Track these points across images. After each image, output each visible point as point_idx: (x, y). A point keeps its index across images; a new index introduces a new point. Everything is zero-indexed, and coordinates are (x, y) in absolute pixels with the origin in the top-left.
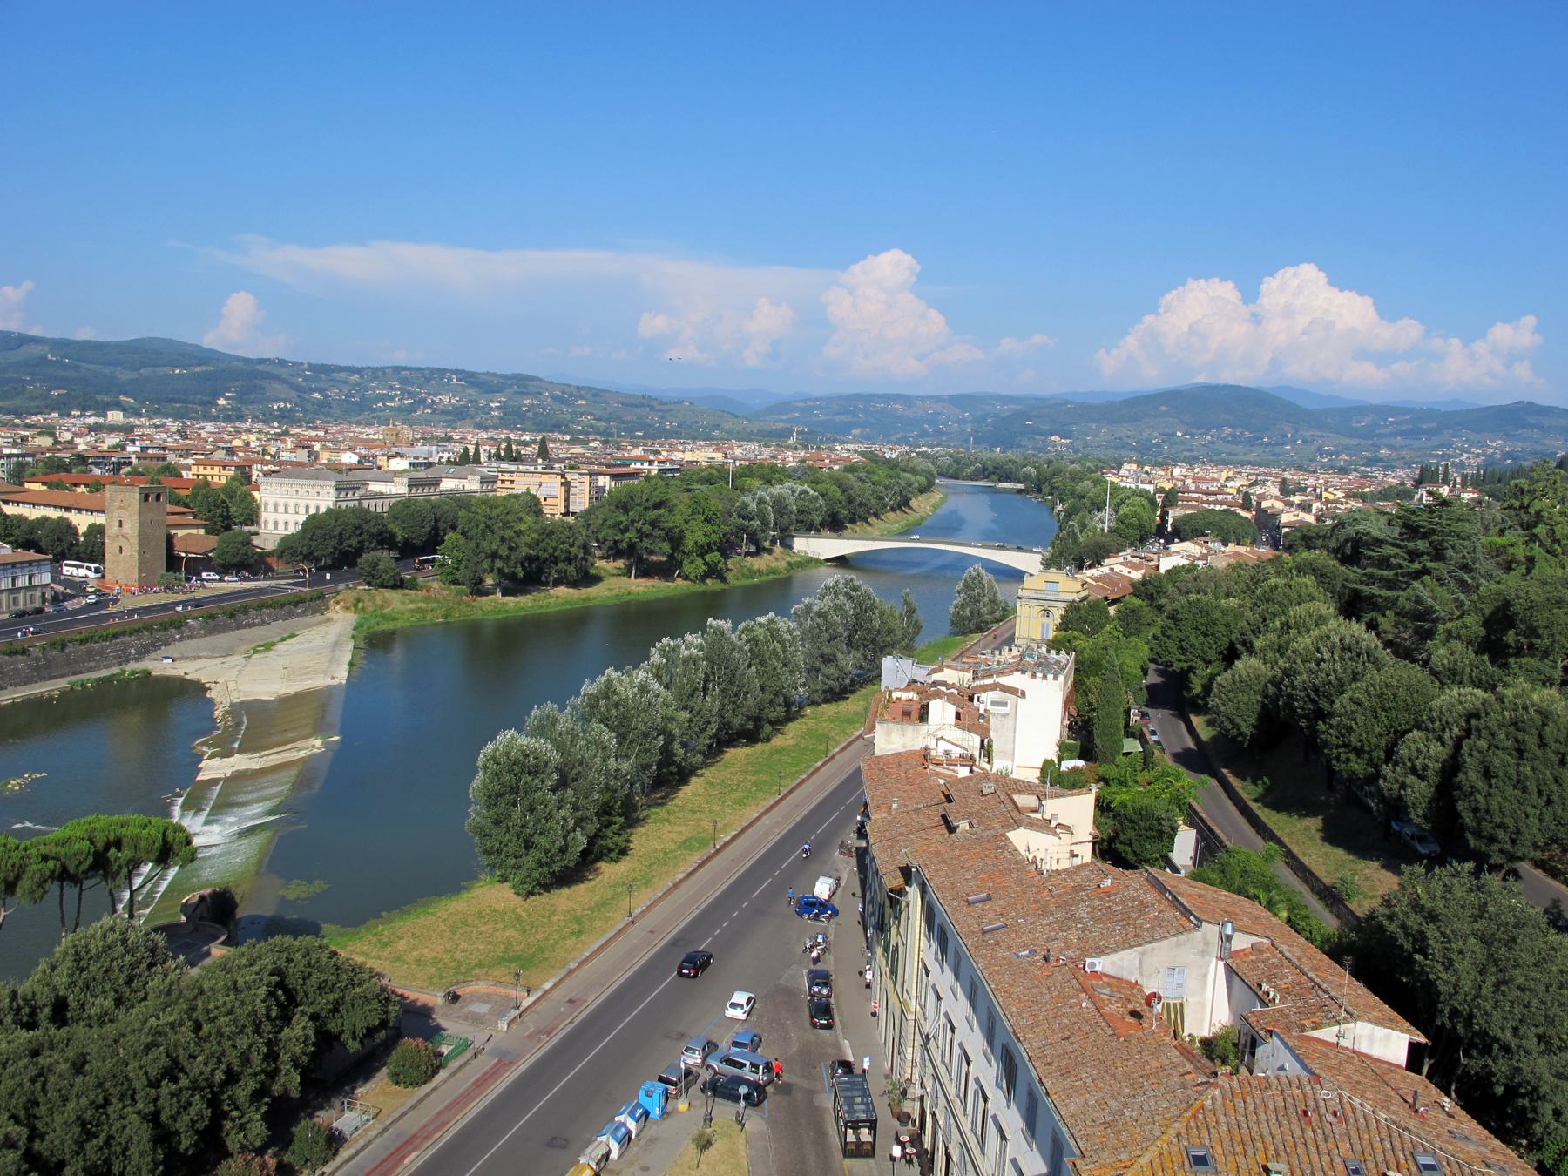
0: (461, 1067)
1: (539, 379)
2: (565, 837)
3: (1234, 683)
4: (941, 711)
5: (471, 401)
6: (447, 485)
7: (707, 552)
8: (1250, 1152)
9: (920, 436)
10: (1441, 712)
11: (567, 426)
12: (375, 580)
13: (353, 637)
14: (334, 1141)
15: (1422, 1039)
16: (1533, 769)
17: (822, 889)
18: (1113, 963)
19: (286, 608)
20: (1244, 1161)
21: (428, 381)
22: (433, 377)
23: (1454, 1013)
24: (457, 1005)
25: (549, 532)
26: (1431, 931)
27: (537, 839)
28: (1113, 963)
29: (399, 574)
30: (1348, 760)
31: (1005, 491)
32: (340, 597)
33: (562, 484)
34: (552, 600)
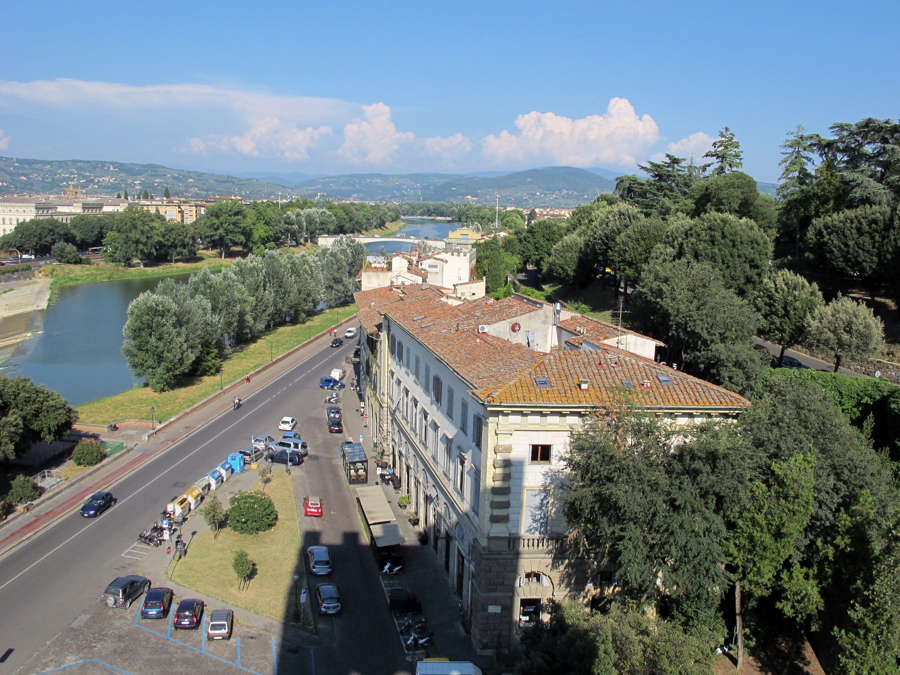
0: (119, 457)
1: (164, 167)
2: (182, 354)
3: (563, 246)
4: (400, 264)
5: (122, 181)
6: (106, 209)
7: (267, 242)
8: (570, 379)
9: (392, 197)
10: (673, 233)
11: (182, 194)
12: (63, 258)
13: (51, 288)
14: (40, 491)
15: (662, 344)
16: (719, 250)
17: (336, 374)
18: (495, 329)
19: (7, 275)
20: (566, 382)
21: (95, 168)
22: (99, 166)
23: (678, 325)
24: (117, 432)
25: (170, 230)
26: (665, 287)
27: (165, 354)
28: (495, 329)
29: (78, 255)
30: (625, 269)
31: (441, 221)
32: (42, 269)
33: (179, 212)
34: (175, 269)
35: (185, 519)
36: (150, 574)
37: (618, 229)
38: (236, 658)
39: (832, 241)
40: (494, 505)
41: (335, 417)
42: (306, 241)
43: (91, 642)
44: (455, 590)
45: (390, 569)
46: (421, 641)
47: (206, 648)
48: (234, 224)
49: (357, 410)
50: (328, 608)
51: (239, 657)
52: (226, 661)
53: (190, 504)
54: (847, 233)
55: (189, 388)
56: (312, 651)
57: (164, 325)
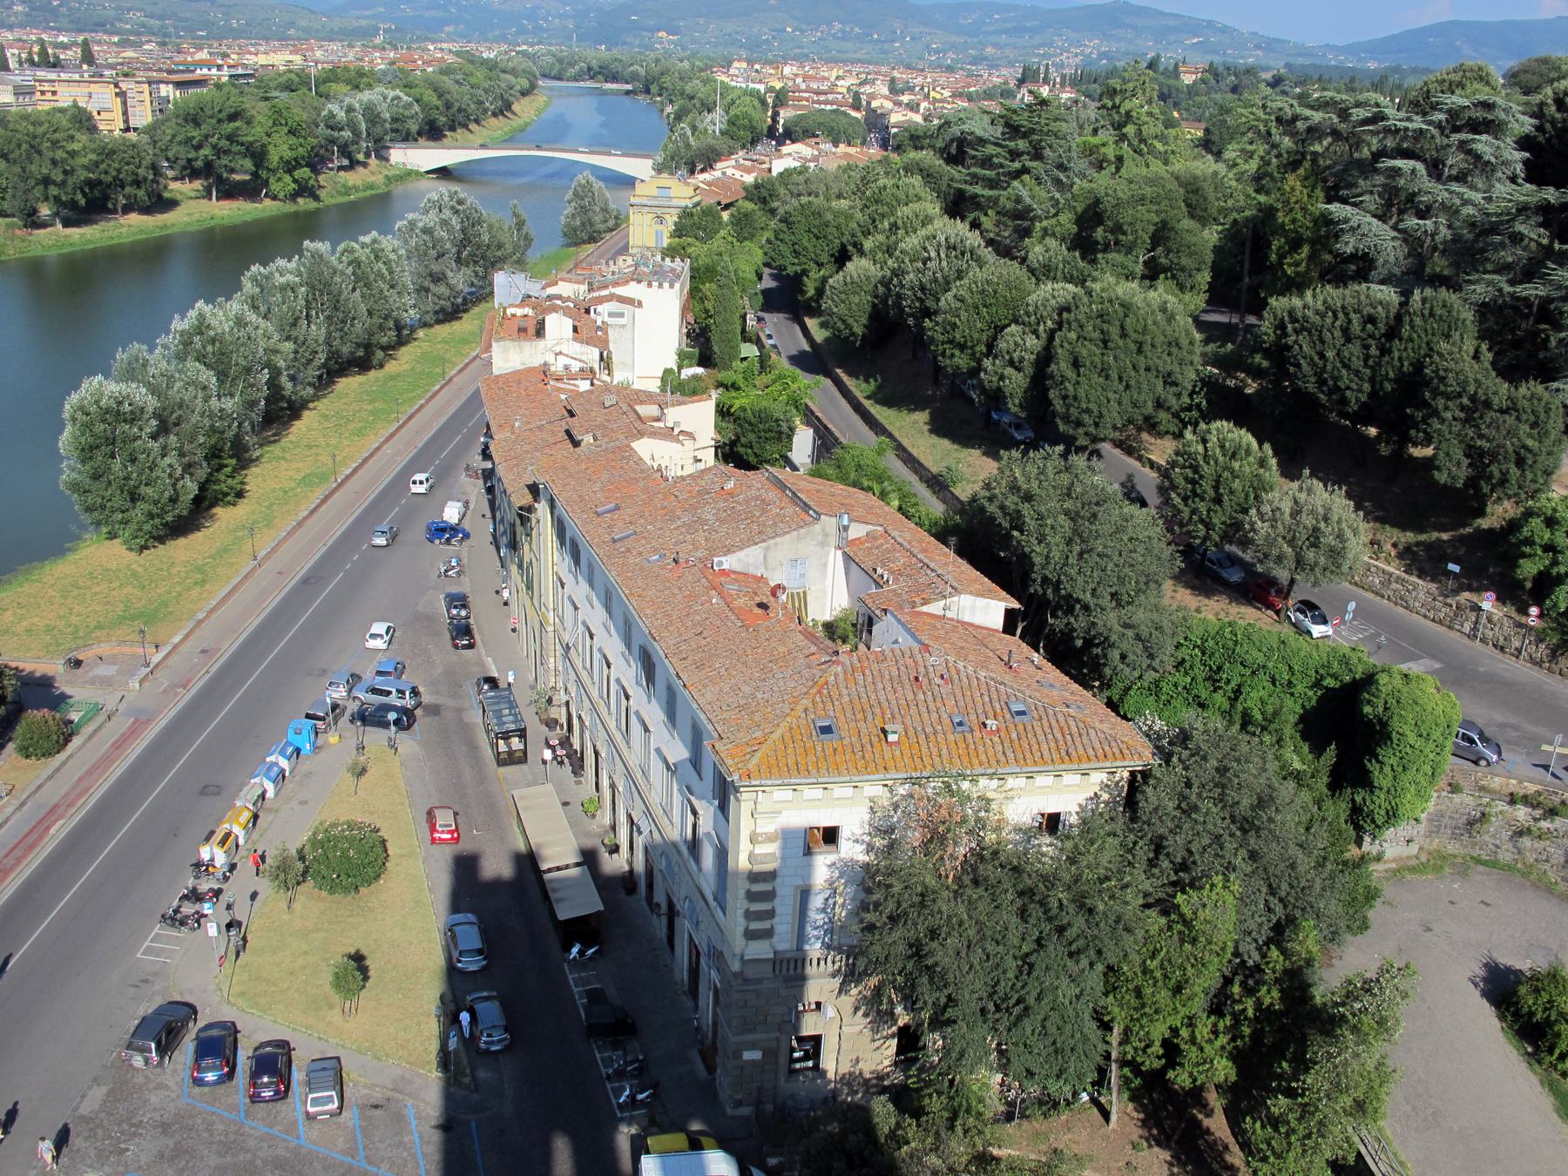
0: (95, 732)
3: (846, 284)
4: (558, 326)
7: (295, 168)
8: (870, 717)
11: (112, 25)
16: (1115, 358)
17: (451, 514)
18: (740, 560)
23: (1045, 580)
24: (80, 671)
25: (108, 152)
26: (1026, 509)
28: (740, 560)
30: (953, 355)
33: (117, 94)
34: (125, 230)
35: (233, 867)
36: (191, 991)
37: (945, 278)
38: (357, 1149)
39: (1301, 347)
40: (752, 897)
41: (458, 614)
42: (368, 155)
43: (119, 1141)
44: (686, 988)
45: (581, 953)
46: (640, 1097)
47: (307, 1136)
48: (231, 138)
49: (497, 592)
50: (492, 1043)
51: (361, 1147)
52: (343, 1158)
53: (237, 837)
54: (1327, 336)
55: (192, 537)
56: (473, 1124)
57: (136, 438)
